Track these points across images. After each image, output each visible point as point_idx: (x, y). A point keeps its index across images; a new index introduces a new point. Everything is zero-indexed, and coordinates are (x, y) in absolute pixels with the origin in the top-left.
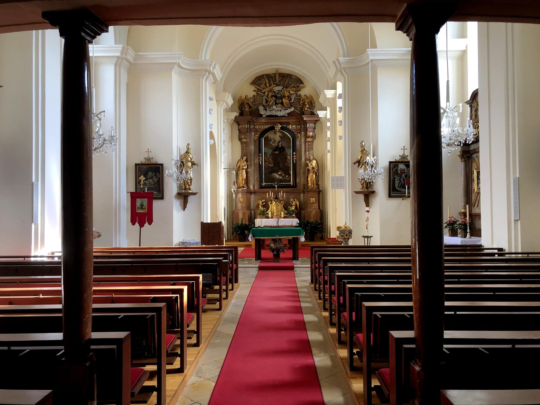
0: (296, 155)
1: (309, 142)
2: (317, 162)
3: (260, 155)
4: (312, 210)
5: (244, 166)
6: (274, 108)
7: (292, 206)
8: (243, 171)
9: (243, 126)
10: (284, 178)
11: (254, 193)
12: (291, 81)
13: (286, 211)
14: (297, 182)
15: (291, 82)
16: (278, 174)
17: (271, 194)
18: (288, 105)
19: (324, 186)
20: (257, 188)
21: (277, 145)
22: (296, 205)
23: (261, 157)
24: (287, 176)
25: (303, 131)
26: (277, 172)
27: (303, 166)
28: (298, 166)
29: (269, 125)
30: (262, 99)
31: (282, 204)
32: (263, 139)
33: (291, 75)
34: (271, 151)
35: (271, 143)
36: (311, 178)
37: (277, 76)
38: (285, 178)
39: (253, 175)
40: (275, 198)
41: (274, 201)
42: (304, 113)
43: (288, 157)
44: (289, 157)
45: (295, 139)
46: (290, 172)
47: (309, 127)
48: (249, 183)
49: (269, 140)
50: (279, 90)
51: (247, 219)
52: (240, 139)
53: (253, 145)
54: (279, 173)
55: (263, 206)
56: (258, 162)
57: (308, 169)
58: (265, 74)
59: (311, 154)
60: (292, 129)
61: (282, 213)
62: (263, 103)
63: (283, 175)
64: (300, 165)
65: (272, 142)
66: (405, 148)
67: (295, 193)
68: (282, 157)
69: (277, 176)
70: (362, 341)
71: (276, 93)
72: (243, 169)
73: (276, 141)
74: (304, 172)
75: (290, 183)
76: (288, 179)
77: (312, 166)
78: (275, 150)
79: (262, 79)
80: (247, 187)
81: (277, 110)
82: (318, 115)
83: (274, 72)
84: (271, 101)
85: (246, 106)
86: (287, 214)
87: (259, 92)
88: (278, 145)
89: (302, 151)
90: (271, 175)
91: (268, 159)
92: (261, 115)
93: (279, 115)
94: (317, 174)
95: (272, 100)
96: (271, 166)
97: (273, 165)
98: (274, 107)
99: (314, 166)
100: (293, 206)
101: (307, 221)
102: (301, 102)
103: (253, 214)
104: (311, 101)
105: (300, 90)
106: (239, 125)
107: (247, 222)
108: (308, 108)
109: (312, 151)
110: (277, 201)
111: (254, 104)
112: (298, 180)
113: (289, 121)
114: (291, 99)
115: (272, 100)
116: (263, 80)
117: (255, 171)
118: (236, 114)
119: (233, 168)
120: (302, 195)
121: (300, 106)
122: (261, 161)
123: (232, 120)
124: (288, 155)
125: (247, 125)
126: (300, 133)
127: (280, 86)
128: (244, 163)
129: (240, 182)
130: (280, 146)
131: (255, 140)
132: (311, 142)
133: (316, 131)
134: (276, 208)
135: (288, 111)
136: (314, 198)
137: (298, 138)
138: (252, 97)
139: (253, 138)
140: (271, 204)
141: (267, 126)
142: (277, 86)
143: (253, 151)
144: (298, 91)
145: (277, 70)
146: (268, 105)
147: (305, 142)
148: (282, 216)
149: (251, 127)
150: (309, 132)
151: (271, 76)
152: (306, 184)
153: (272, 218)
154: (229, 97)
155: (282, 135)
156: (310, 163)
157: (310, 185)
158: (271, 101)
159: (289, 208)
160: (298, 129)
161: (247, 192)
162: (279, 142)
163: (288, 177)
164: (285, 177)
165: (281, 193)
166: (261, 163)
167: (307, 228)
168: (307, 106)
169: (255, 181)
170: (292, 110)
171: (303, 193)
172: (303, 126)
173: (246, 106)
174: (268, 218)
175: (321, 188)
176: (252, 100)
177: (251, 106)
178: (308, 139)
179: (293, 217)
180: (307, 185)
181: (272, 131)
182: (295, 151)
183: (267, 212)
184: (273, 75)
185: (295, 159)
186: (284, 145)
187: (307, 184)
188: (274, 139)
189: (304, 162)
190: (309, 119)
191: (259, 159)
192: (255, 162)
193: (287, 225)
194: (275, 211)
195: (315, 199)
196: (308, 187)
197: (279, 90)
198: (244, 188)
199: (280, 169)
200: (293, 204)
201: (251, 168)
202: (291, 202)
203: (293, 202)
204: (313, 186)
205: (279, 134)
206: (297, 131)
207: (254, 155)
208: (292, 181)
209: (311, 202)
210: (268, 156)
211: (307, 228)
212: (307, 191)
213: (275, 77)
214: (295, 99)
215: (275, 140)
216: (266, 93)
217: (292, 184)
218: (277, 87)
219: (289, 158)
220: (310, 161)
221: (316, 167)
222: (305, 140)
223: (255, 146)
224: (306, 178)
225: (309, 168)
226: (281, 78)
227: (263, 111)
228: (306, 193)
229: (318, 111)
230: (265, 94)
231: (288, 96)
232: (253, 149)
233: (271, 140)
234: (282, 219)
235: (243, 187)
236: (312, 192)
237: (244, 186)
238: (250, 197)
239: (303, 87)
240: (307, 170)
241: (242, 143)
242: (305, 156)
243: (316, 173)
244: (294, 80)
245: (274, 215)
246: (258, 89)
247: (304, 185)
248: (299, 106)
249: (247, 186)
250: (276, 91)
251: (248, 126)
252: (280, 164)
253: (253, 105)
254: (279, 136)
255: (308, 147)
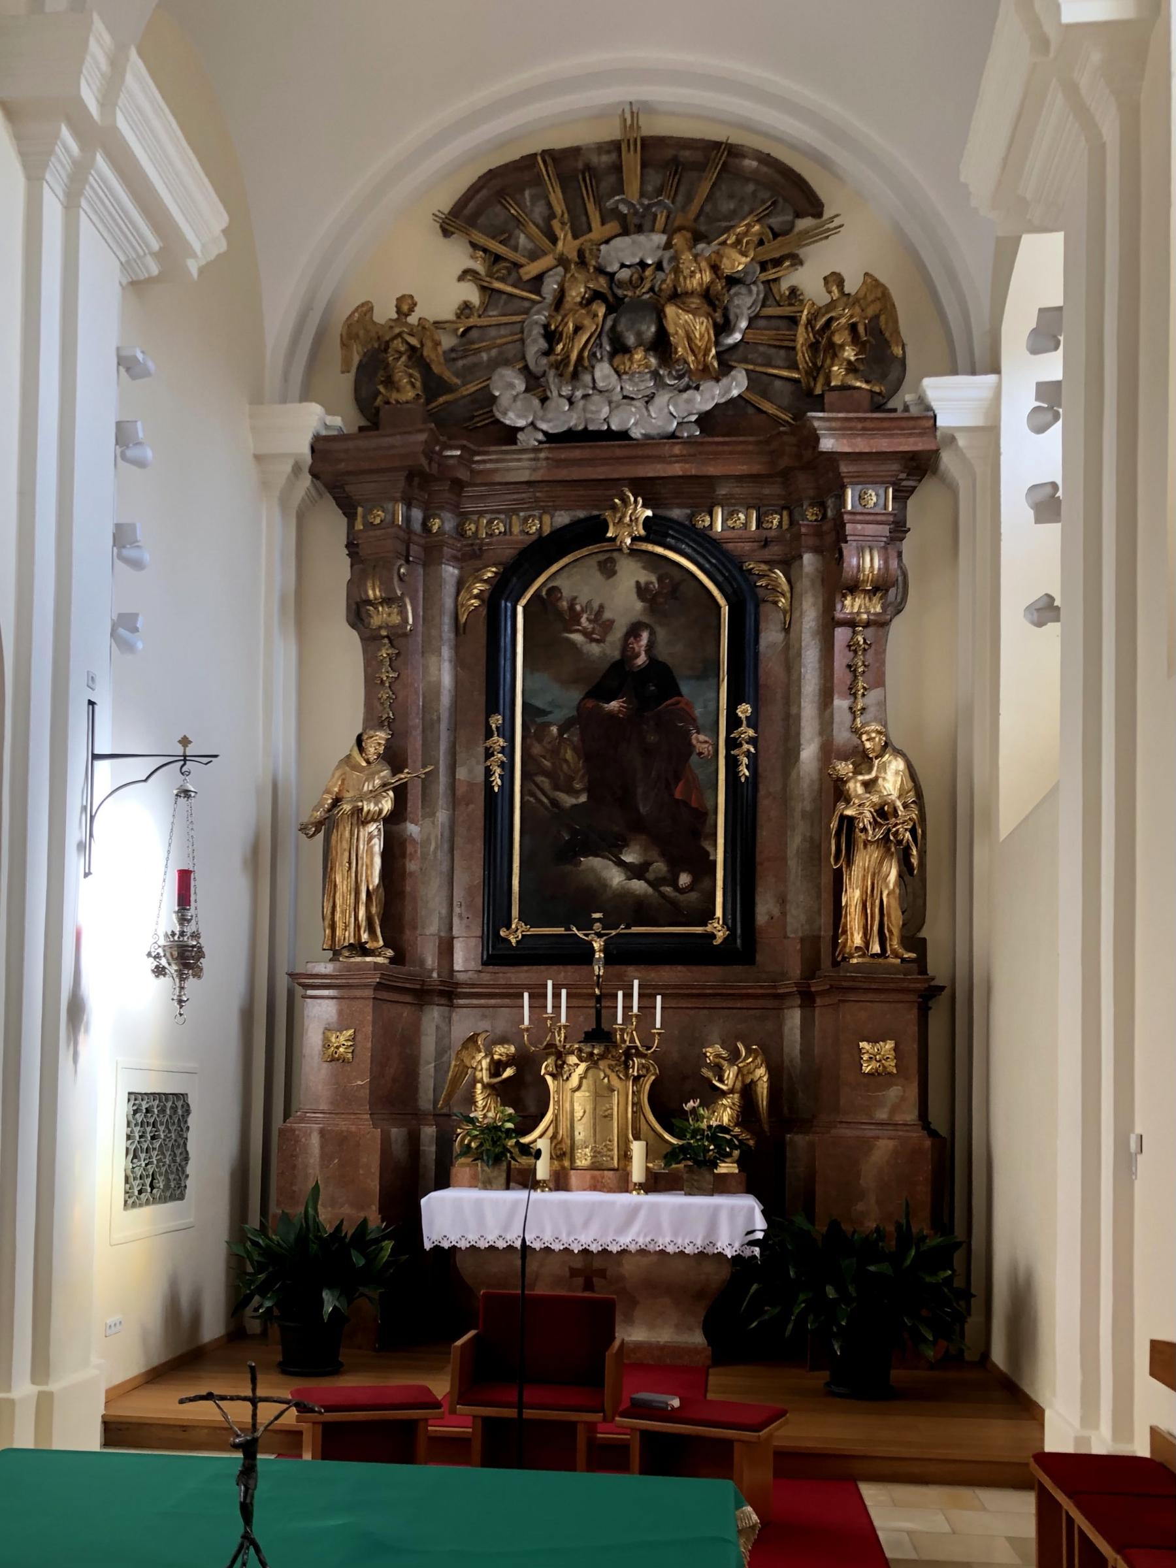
0: (753, 722)
1: (851, 623)
2: (909, 766)
3: (496, 720)
4: (870, 1132)
5: (375, 795)
6: (600, 384)
7: (711, 1096)
8: (364, 833)
9: (378, 516)
10: (663, 895)
11: (442, 993)
12: (731, 196)
13: (667, 1136)
14: (761, 918)
15: (732, 206)
16: (621, 864)
17: (556, 1007)
18: (707, 351)
19: (961, 955)
20: (464, 958)
21: (617, 655)
22: (747, 1091)
23: (499, 742)
24: (684, 879)
25: (816, 550)
26: (611, 848)
27: (808, 805)
28: (767, 807)
29: (568, 509)
30: (518, 327)
31: (636, 1079)
32: (520, 609)
33: (733, 151)
34: (575, 695)
35: (577, 637)
36: (864, 892)
37: (632, 161)
38: (668, 890)
39: (445, 867)
40: (590, 1037)
41: (581, 1060)
42: (823, 404)
43: (700, 740)
44: (702, 737)
45: (750, 607)
46: (710, 849)
47: (859, 509)
48: (415, 928)
49: (559, 614)
50: (643, 265)
51: (374, 1185)
52: (358, 614)
53: (446, 652)
54: (629, 858)
55: (503, 1092)
56: (481, 778)
57: (843, 817)
58: (544, 151)
59: (868, 716)
60: (729, 534)
61: (637, 1149)
62: (524, 358)
63: (659, 867)
64: (785, 799)
65: (585, 633)
66: (249, 1393)
67: (745, 1004)
68: (652, 738)
69: (616, 877)
70: (799, 1060)
71: (621, 285)
72: (360, 818)
73: (612, 622)
74: (814, 853)
75: (709, 928)
76: (693, 896)
77: (875, 799)
78: (601, 690)
79: (522, 191)
80: (390, 953)
81: (625, 397)
82: (929, 408)
83: (611, 131)
84: (578, 329)
85: (402, 372)
86: (672, 1155)
87: (502, 280)
88: (627, 655)
89: (799, 693)
90: (568, 868)
91: (555, 752)
92: (510, 435)
93: (636, 433)
94: (915, 861)
95: (587, 322)
96: (568, 801)
97: (583, 798)
98: (603, 372)
99: (895, 794)
100: (724, 1094)
101: (834, 1225)
102: (802, 336)
103: (429, 1149)
104: (874, 328)
105: (797, 261)
106: (348, 507)
107: (375, 1208)
108: (851, 368)
109: (873, 696)
110: (602, 1057)
111: (460, 363)
112: (765, 908)
113: (711, 470)
114: (726, 316)
115: (587, 322)
116: (534, 199)
117: (459, 841)
118: (324, 433)
119: (179, 750)
120: (794, 1018)
121: (794, 366)
122: (502, 765)
123: (297, 469)
124: (700, 722)
125: (409, 506)
126: (788, 564)
127: (652, 230)
128: (370, 777)
129: (338, 915)
130: (642, 660)
131: (463, 619)
132: (867, 625)
133: (907, 545)
134: (589, 1108)
135: (709, 396)
136: (890, 1045)
137: (776, 603)
138: (452, 317)
139: (449, 603)
140: (554, 1076)
141: (547, 519)
142: (625, 232)
143: (446, 700)
144: (777, 262)
145: (633, 113)
146: (560, 366)
147: (829, 623)
148: (637, 1173)
149: (436, 525)
150: (860, 552)
151: (588, 168)
152: (826, 933)
153: (560, 1182)
154: (129, 78)
155: (660, 580)
156: (857, 772)
157: (858, 940)
158: (578, 329)
159: (694, 1110)
160: (773, 533)
161: (379, 987)
162: (634, 631)
163: (691, 888)
164: (674, 883)
165: (628, 996)
166: (497, 781)
167: (831, 1292)
168: (849, 353)
169: (457, 910)
170: (735, 393)
171: (800, 1006)
172: (811, 514)
173: (402, 372)
174: (528, 1181)
175: (936, 965)
176: (448, 341)
177: (440, 378)
178: (852, 605)
179: (721, 1186)
180: (835, 944)
181: (584, 551)
182: (750, 690)
183: (525, 1140)
184: (605, 159)
185: (748, 754)
186: (672, 651)
187: (835, 937)
188: (601, 607)
189: (815, 776)
190: (862, 445)
191: (489, 754)
192: (462, 774)
193: (671, 1249)
194: (582, 1132)
195: (896, 1049)
196: (844, 959)
197: (643, 265)
198: (368, 959)
199: (637, 827)
200: (721, 1080)
201: (428, 821)
202: (708, 1066)
203: (725, 1064)
204: (876, 948)
205: (631, 574)
206: (767, 554)
207: (454, 728)
208: (719, 913)
209: (867, 1068)
210: (554, 729)
211: (831, 1292)
212: (833, 989)
213: (617, 168)
214: (762, 323)
215: (607, 615)
216: (551, 286)
217: (721, 935)
218: (627, 240)
219: (706, 749)
220: (863, 760)
221: (905, 806)
222: (828, 609)
223: (459, 662)
224: (827, 896)
225: (849, 812)
226: (655, 179)
227: (519, 403)
228: (828, 1000)
229: (927, 382)
230: (539, 293)
231: (708, 296)
232: (447, 679)
233: (575, 617)
234: (634, 1198)
235: (360, 949)
236: (870, 996)
237: (365, 937)
238: (419, 1019)
239: (822, 234)
240: (834, 825)
241: (370, 639)
242: (821, 733)
243: (907, 852)
244: (751, 187)
245: (578, 1163)
246: (498, 258)
247: (811, 943)
248: (785, 373)
249: (386, 945)
250: (623, 266)
251: (417, 514)
252: (640, 790)
253: (457, 375)
254: (638, 583)
255: (846, 661)
